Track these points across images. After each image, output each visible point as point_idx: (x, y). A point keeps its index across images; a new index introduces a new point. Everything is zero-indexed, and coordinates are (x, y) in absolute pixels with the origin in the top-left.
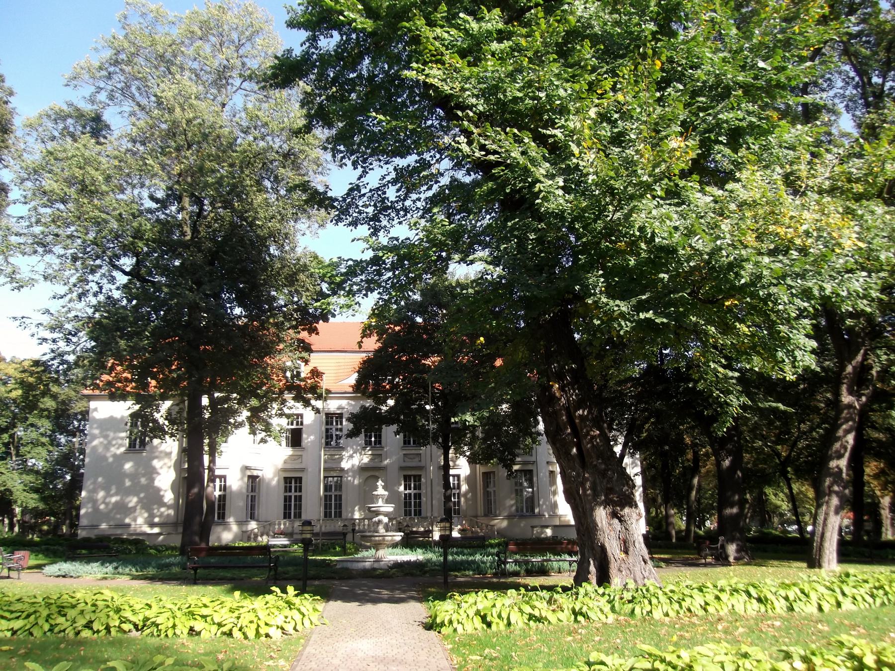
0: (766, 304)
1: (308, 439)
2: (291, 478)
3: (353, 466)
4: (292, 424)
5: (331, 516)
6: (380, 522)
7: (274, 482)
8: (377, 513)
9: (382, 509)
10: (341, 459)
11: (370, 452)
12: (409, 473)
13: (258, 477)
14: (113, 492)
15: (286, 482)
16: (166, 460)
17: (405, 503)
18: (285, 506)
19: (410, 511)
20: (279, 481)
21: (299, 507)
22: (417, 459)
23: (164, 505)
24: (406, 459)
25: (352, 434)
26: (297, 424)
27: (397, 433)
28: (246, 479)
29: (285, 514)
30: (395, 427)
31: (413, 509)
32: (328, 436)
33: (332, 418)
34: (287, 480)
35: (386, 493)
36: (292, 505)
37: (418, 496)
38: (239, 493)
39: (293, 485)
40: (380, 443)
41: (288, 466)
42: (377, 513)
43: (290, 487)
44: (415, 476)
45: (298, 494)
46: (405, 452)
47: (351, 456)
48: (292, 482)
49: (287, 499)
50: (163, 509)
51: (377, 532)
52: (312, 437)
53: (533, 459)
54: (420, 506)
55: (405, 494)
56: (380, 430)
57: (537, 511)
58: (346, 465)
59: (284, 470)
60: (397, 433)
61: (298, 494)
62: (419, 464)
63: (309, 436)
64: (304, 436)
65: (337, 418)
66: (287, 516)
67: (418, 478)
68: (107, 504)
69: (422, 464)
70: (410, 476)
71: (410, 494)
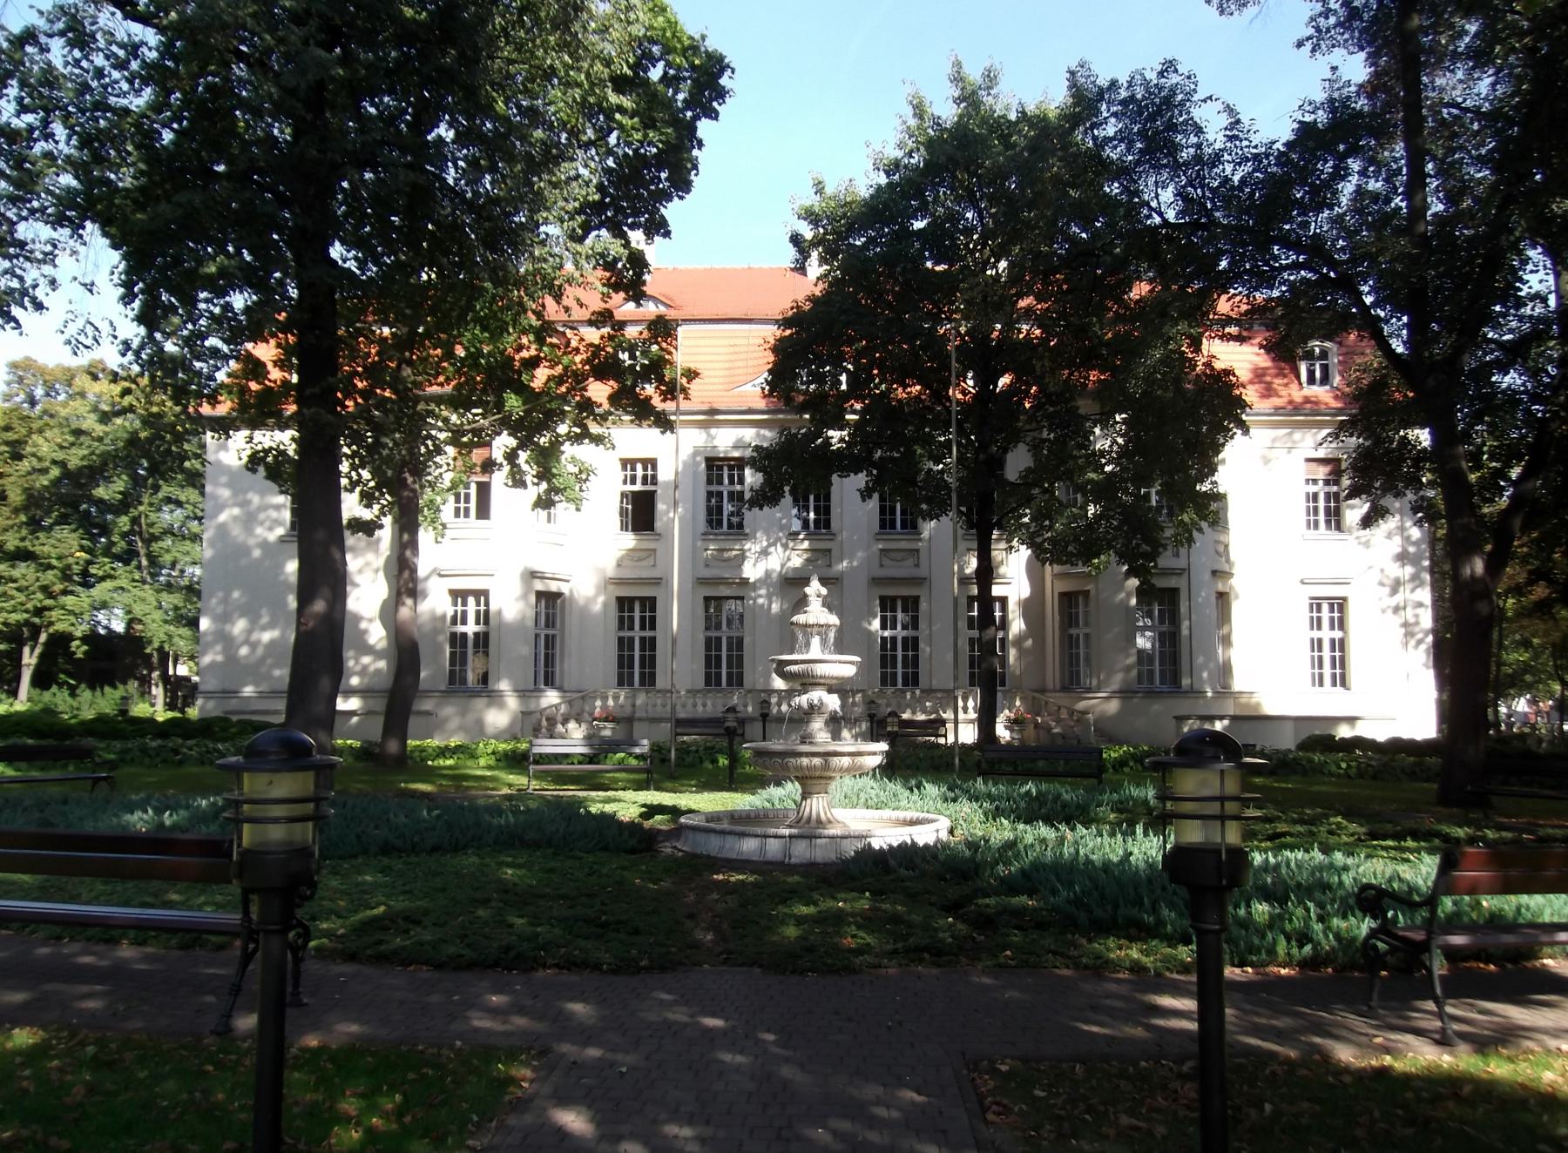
2: (631, 600)
3: (768, 573)
4: (633, 482)
7: (597, 607)
8: (806, 682)
9: (820, 669)
10: (742, 557)
11: (806, 544)
13: (559, 595)
14: (265, 620)
15: (621, 609)
16: (370, 556)
17: (884, 658)
20: (605, 605)
21: (649, 662)
22: (910, 562)
23: (369, 650)
24: (886, 562)
25: (766, 497)
27: (866, 494)
28: (533, 598)
30: (860, 479)
33: (720, 468)
34: (624, 603)
35: (834, 620)
36: (637, 660)
37: (912, 644)
38: (519, 626)
39: (637, 614)
40: (828, 525)
41: (628, 574)
43: (631, 619)
44: (905, 599)
45: (648, 634)
47: (765, 553)
48: (635, 607)
49: (624, 644)
50: (366, 660)
51: (806, 739)
53: (1181, 563)
55: (884, 639)
57: (1186, 682)
58: (752, 571)
59: (619, 582)
60: (866, 494)
65: (731, 468)
66: (624, 680)
67: (911, 604)
68: (254, 646)
69: (922, 572)
70: (894, 599)
71: (894, 639)
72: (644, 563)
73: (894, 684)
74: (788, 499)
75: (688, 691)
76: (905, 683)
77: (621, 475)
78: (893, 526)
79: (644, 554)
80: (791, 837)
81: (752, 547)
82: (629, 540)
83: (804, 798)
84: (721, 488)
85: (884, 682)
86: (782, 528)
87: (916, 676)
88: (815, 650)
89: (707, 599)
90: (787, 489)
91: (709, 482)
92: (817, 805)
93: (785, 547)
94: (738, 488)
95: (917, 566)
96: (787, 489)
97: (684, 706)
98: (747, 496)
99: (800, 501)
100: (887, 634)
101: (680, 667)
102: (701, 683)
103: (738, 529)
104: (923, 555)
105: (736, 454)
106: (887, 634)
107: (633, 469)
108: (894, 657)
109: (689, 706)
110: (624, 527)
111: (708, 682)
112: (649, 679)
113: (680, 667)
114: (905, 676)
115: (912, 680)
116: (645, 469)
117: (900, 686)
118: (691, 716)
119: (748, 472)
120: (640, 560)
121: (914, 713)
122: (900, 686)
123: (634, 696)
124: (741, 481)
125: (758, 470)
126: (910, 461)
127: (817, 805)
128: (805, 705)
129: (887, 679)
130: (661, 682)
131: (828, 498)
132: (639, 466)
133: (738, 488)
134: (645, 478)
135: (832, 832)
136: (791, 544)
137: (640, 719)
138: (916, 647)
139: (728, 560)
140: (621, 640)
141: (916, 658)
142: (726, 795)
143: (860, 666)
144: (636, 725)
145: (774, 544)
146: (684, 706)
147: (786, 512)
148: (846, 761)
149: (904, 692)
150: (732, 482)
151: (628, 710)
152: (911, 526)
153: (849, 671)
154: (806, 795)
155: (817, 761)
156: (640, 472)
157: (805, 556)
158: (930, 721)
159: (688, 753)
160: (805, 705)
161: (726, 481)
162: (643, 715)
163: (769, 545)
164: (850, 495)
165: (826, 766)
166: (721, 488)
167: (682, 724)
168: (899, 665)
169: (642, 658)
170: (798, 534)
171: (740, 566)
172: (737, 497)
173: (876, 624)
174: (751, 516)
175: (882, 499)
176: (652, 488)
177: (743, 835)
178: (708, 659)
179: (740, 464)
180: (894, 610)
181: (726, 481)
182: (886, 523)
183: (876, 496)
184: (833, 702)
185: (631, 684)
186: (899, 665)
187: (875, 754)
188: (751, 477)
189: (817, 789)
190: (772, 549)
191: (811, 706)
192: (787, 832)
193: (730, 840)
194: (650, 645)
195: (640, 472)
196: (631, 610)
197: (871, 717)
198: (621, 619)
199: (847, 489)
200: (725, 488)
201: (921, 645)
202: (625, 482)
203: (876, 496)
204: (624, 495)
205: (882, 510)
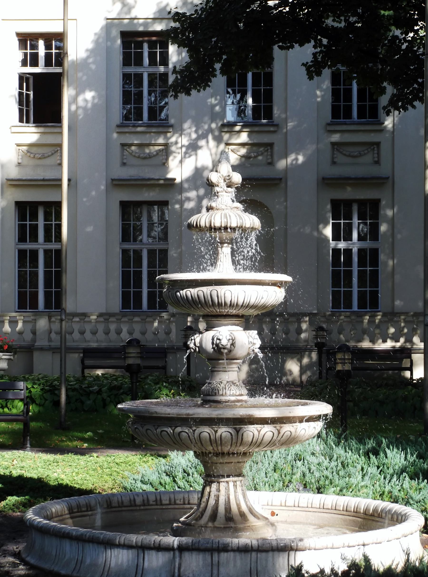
0: (136, 382)
1: (75, 100)
4: (35, 63)
5: (138, 304)
6: (220, 355)
8: (214, 313)
9: (228, 294)
11: (244, 137)
12: (348, 193)
15: (22, 216)
17: (336, 275)
18: (21, 277)
19: (349, 295)
21: (55, 279)
22: (368, 158)
24: (340, 158)
25: (193, 78)
26: (48, 63)
27: (313, 70)
29: (22, 297)
30: (306, 52)
31: (355, 289)
32: (131, 96)
33: (140, 45)
35: (252, 221)
37: (370, 257)
39: (41, 223)
40: (269, 115)
41: (29, 174)
42: (214, 313)
43: (34, 228)
44: (362, 203)
45: (28, 246)
46: (336, 138)
47: (193, 147)
51: (210, 399)
52: (89, 95)
54: (375, 281)
55: (336, 252)
56: (269, 60)
60: (313, 70)
61: (28, 246)
62: (374, 171)
63: (80, 91)
64: (67, 94)
65: (152, 45)
66: (26, 301)
67: (370, 211)
69: (384, 170)
70: (348, 203)
71: (348, 252)
72: (48, 161)
73: (349, 305)
74: (219, 81)
75: (100, 315)
76: (362, 305)
77: (19, 55)
78: (348, 114)
79: (47, 151)
80: (182, 549)
81: (180, 141)
82: (31, 134)
83: (208, 483)
84: (139, 70)
85: (336, 304)
86: (214, 117)
87: (375, 296)
88: (224, 267)
89: (125, 206)
90: (218, 66)
91: (126, 62)
92: (230, 492)
93: (218, 140)
94: (162, 69)
95: (377, 163)
96: (218, 66)
97: (94, 333)
98: (171, 79)
99: (236, 85)
100: (342, 245)
101: (92, 284)
102: (116, 304)
103: (159, 122)
104: (385, 148)
105: (159, 27)
106: (342, 245)
107: (34, 47)
108: (349, 274)
109: (100, 335)
110: (24, 117)
111: (125, 303)
112: (55, 301)
113: (92, 284)
114: (362, 295)
115: (369, 301)
116: (48, 47)
117: (355, 307)
118: (104, 345)
119: (172, 49)
120: (43, 157)
121: (373, 341)
122: (355, 307)
123: (35, 321)
124: (165, 61)
125: (181, 44)
126: (376, 27)
127: (230, 492)
128: (209, 347)
129: (340, 300)
130: (69, 304)
131: (269, 79)
132: (41, 43)
133: (162, 69)
134: (48, 57)
135: (245, 539)
136: (226, 137)
137: (41, 349)
138: (375, 261)
139: (150, 156)
140: (22, 254)
141: (375, 275)
142: (121, 456)
143: (290, 289)
144: (36, 355)
145: (204, 136)
146: (94, 333)
147: (219, 99)
148: (267, 431)
149: (360, 316)
150: (153, 62)
151: (28, 336)
152: (371, 114)
153: (274, 296)
154: (210, 478)
155: (223, 431)
156: (42, 51)
157: (243, 151)
158: (394, 350)
159: (88, 394)
160: (209, 347)
161: (146, 61)
162: (44, 343)
163: (199, 138)
164: (298, 79)
165: (238, 437)
166: (139, 70)
167: (92, 355)
168: (355, 280)
169: (47, 274)
170: (234, 124)
171: (164, 165)
172: (159, 81)
173: (328, 232)
174: (174, 105)
175: (335, 79)
176: (58, 70)
177: (110, 544)
178: (125, 276)
179: (162, 39)
180: (349, 217)
181: (146, 61)
182: (339, 110)
183: (327, 72)
184: (248, 341)
185: (34, 305)
186: (355, 280)
187: (311, 419)
188: (176, 54)
189: (226, 469)
190: (202, 143)
191: (218, 349)
192: (174, 541)
193: (90, 548)
194: (56, 258)
195: (42, 51)
196: (34, 217)
197: (320, 347)
198: (22, 229)
199: (291, 62)
200: (145, 70)
201: (382, 257)
202: (24, 63)
203: (327, 72)
204: (22, 78)
205: (335, 93)
